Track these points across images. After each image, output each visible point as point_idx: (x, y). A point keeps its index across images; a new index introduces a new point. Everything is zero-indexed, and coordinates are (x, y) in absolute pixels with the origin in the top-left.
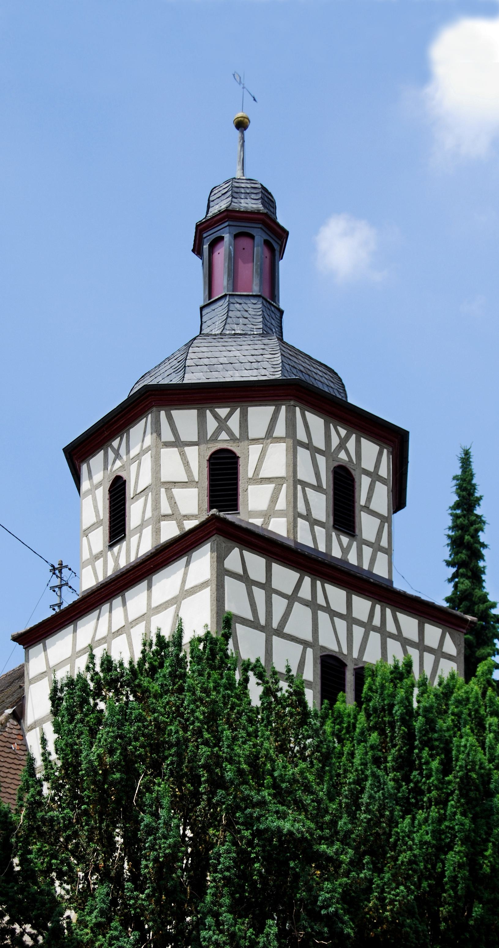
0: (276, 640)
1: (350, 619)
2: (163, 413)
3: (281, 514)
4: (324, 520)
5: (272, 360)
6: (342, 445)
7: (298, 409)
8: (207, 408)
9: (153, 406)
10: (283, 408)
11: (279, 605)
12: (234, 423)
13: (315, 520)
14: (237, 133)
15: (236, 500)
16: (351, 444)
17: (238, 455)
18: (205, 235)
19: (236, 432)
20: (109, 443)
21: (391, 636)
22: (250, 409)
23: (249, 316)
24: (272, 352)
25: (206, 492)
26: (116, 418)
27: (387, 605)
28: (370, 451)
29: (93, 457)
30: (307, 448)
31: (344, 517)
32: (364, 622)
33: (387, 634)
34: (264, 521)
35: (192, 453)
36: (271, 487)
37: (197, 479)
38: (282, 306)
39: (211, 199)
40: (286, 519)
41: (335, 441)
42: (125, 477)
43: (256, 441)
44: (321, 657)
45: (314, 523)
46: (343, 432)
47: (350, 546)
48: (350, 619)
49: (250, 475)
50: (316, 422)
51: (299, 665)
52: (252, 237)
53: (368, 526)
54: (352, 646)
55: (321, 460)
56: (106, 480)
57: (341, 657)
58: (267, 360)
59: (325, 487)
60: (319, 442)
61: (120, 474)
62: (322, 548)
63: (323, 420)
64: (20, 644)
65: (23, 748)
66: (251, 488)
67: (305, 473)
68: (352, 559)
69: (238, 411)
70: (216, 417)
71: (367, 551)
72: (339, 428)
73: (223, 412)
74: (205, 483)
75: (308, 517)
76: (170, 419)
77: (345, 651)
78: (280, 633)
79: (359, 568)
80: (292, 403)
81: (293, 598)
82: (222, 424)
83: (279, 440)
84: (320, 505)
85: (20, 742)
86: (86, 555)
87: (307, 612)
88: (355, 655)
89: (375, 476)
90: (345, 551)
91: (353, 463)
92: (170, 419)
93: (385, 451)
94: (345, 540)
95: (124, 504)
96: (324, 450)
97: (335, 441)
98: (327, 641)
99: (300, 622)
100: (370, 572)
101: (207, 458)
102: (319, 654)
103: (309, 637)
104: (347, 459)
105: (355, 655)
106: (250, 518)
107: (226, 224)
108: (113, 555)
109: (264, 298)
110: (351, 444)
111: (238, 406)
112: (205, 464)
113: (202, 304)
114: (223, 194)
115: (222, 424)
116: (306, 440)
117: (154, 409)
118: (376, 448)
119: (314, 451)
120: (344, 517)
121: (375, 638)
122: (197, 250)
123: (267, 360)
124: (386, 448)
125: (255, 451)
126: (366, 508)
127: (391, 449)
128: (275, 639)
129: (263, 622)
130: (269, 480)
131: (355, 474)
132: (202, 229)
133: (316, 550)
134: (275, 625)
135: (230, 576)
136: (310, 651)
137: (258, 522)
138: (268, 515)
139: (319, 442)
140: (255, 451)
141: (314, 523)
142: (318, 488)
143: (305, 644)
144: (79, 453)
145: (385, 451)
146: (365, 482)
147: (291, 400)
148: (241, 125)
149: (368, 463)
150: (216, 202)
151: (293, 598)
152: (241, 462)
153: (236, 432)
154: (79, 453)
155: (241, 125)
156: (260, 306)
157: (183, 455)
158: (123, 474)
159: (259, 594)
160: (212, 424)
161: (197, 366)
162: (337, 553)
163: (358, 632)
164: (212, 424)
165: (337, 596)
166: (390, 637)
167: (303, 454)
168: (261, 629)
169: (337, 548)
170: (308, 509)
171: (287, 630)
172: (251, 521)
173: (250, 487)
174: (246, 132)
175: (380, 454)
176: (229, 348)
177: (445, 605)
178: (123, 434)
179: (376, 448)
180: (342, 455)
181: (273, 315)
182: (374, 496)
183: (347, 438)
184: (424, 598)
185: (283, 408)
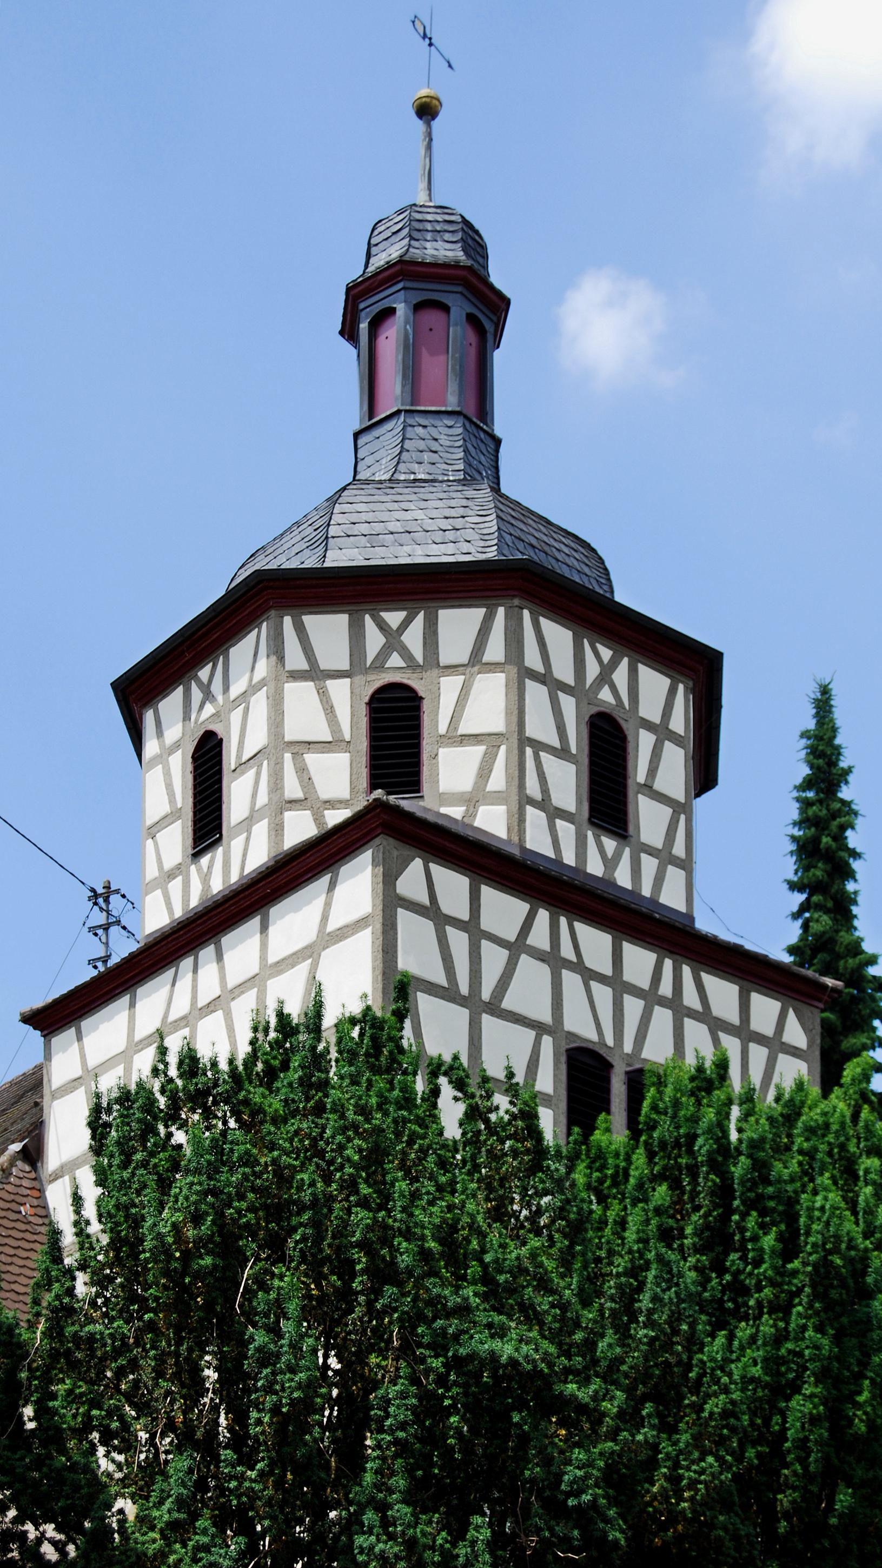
1: (619, 985)
3: (496, 798)
5: (482, 526)
6: (605, 677)
7: (526, 613)
8: (367, 611)
10: (501, 611)
11: (494, 959)
12: (413, 638)
13: (557, 809)
14: (420, 125)
15: (418, 774)
16: (621, 676)
17: (421, 694)
18: (362, 306)
19: (418, 653)
20: (193, 673)
23: (440, 448)
25: (363, 760)
26: (204, 630)
28: (654, 685)
29: (164, 697)
30: (543, 683)
31: (608, 803)
33: (685, 1011)
34: (467, 810)
35: (340, 690)
36: (478, 751)
38: (498, 431)
39: (373, 241)
41: (592, 670)
42: (221, 733)
43: (452, 669)
45: (555, 814)
46: (606, 654)
47: (618, 855)
48: (619, 985)
49: (442, 728)
50: (559, 636)
51: (528, 1066)
52: (446, 309)
53: (650, 820)
55: (568, 704)
57: (602, 1052)
58: (473, 526)
59: (574, 751)
60: (564, 671)
61: (212, 727)
62: (569, 858)
63: (570, 633)
64: (35, 1029)
65: (41, 1212)
66: (444, 753)
67: (540, 726)
68: (623, 878)
69: (421, 616)
70: (382, 626)
71: (649, 864)
72: (600, 647)
73: (394, 618)
74: (363, 744)
76: (300, 630)
77: (610, 1041)
78: (494, 1008)
79: (635, 893)
80: (516, 602)
81: (517, 948)
82: (393, 639)
83: (493, 667)
85: (35, 1202)
86: (151, 871)
87: (543, 972)
88: (628, 1047)
89: (662, 732)
90: (611, 863)
91: (625, 709)
92: (300, 630)
93: (681, 687)
94: (610, 844)
95: (220, 781)
97: (592, 670)
98: (579, 1023)
99: (530, 990)
100: (654, 901)
101: (367, 699)
102: (564, 1046)
103: (545, 1016)
105: (628, 1047)
106: (441, 805)
107: (400, 286)
109: (466, 417)
110: (621, 676)
111: (421, 608)
112: (363, 711)
113: (357, 427)
114: (394, 233)
115: (393, 639)
118: (665, 682)
119: (555, 686)
120: (608, 803)
121: (662, 1017)
122: (349, 331)
123: (473, 526)
124: (682, 682)
125: (450, 686)
126: (647, 788)
127: (691, 684)
129: (464, 989)
130: (475, 738)
131: (627, 727)
132: (356, 294)
133: (558, 862)
134: (486, 995)
135: (407, 909)
136: (547, 1041)
137: (456, 812)
138: (473, 800)
139: (564, 671)
140: (450, 686)
142: (562, 753)
143: (539, 1028)
144: (139, 691)
145: (681, 687)
146: (645, 741)
147: (514, 596)
148: (426, 111)
149: (650, 709)
151: (517, 948)
152: (426, 706)
154: (139, 691)
155: (426, 111)
156: (460, 430)
157: (323, 694)
158: (217, 728)
159: (458, 941)
160: (374, 640)
161: (349, 536)
162: (595, 867)
163: (633, 1007)
164: (374, 640)
165: (595, 943)
166: (689, 1016)
167: (536, 693)
168: (462, 1001)
169: (596, 858)
170: (545, 790)
171: (507, 1004)
172: (443, 810)
173: (442, 751)
174: (435, 124)
175: (672, 692)
176: (405, 505)
177: (787, 959)
178: (217, 658)
179: (664, 682)
180: (605, 695)
181: (483, 447)
183: (614, 663)
184: (749, 946)
185: (501, 611)
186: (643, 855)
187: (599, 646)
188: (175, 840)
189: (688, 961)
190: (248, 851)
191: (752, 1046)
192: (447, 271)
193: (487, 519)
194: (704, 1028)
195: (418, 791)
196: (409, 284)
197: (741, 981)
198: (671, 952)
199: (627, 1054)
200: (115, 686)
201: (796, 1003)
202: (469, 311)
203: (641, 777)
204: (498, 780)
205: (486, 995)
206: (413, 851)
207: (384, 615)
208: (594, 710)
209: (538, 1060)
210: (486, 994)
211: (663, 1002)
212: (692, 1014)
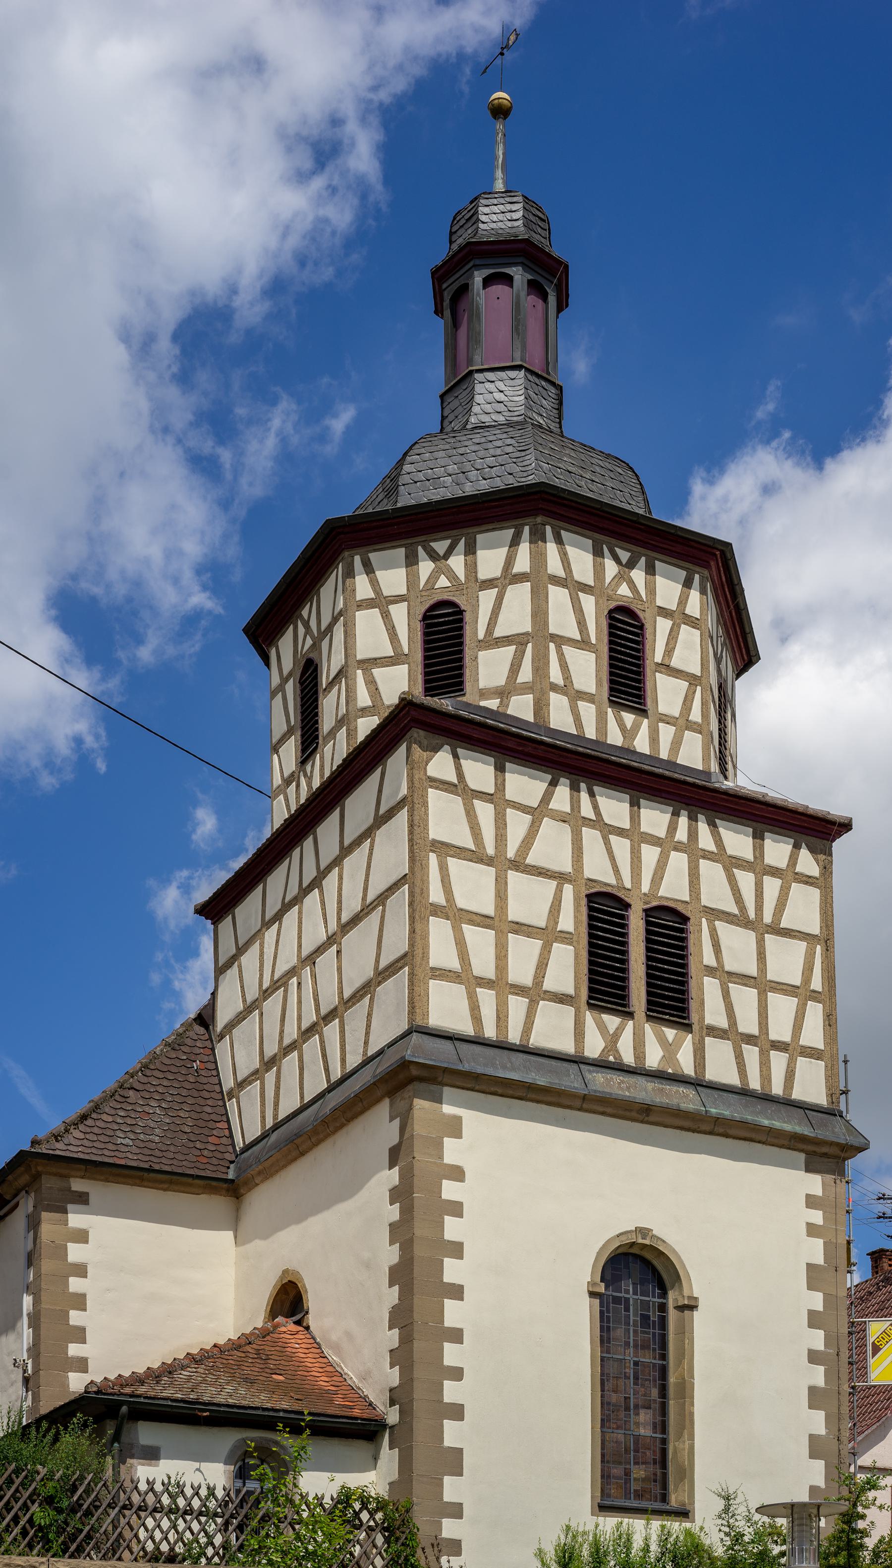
0: (514, 877)
1: (637, 837)
2: (357, 559)
3: (526, 688)
4: (593, 690)
5: (521, 459)
8: (418, 543)
9: (343, 549)
11: (517, 825)
13: (577, 692)
17: (463, 608)
18: (444, 286)
19: (461, 573)
20: (297, 613)
21: (707, 855)
22: (479, 537)
23: (506, 399)
24: (523, 448)
27: (699, 810)
28: (666, 589)
29: (282, 636)
30: (565, 586)
31: (627, 681)
32: (659, 838)
33: (701, 853)
34: (501, 702)
35: (399, 612)
37: (406, 651)
39: (454, 229)
40: (531, 695)
42: (317, 660)
43: (488, 584)
44: (587, 896)
45: (576, 696)
46: (624, 556)
47: (636, 727)
48: (637, 837)
49: (481, 635)
51: (550, 911)
53: (667, 693)
54: (639, 875)
56: (296, 668)
57: (620, 894)
58: (514, 460)
59: (594, 641)
61: (311, 655)
62: (591, 733)
64: (207, 919)
65: (211, 1066)
68: (641, 744)
69: (462, 542)
71: (666, 733)
73: (441, 546)
74: (419, 656)
75: (567, 689)
77: (628, 884)
78: (519, 865)
79: (653, 759)
80: (539, 519)
81: (538, 813)
84: (587, 669)
85: (206, 1059)
86: (277, 780)
87: (565, 832)
88: (645, 888)
90: (629, 734)
91: (642, 601)
94: (629, 718)
95: (316, 700)
96: (592, 584)
98: (597, 869)
99: (552, 846)
100: (671, 764)
101: (420, 617)
102: (584, 892)
103: (567, 867)
104: (618, 550)
105: (645, 888)
106: (480, 700)
107: (471, 264)
108: (305, 775)
109: (527, 370)
111: (462, 535)
112: (418, 626)
113: (444, 390)
114: (468, 220)
116: (561, 573)
117: (346, 554)
120: (627, 681)
121: (678, 861)
122: (438, 311)
123: (514, 460)
124: (698, 573)
125: (487, 599)
126: (666, 668)
128: (512, 876)
129: (490, 850)
131: (646, 617)
132: (440, 275)
133: (581, 738)
134: (511, 853)
136: (568, 889)
137: (493, 704)
138: (503, 693)
140: (487, 599)
141: (576, 696)
142: (583, 644)
143: (561, 878)
144: (264, 630)
146: (663, 626)
147: (536, 515)
150: (459, 233)
151: (538, 813)
152: (468, 617)
153: (461, 573)
154: (264, 630)
156: (522, 381)
157: (386, 616)
159: (485, 812)
161: (416, 482)
162: (615, 738)
163: (650, 855)
165: (614, 807)
166: (704, 858)
167: (558, 596)
168: (489, 861)
169: (615, 730)
171: (531, 859)
172: (483, 703)
173: (481, 654)
176: (461, 451)
178: (313, 597)
181: (544, 393)
182: (681, 647)
186: (661, 725)
187: (618, 550)
188: (290, 750)
189: (704, 811)
190: (334, 753)
191: (767, 879)
192: (508, 246)
193: (528, 452)
194: (719, 867)
195: (462, 690)
196: (478, 262)
197: (754, 824)
198: (687, 804)
199: (645, 894)
200: (246, 630)
201: (812, 839)
202: (530, 277)
203: (658, 658)
204: (526, 674)
205: (768, 918)
206: (442, 739)
207: (433, 545)
208: (613, 605)
209: (560, 905)
210: (511, 853)
211: (679, 847)
212: (707, 855)
